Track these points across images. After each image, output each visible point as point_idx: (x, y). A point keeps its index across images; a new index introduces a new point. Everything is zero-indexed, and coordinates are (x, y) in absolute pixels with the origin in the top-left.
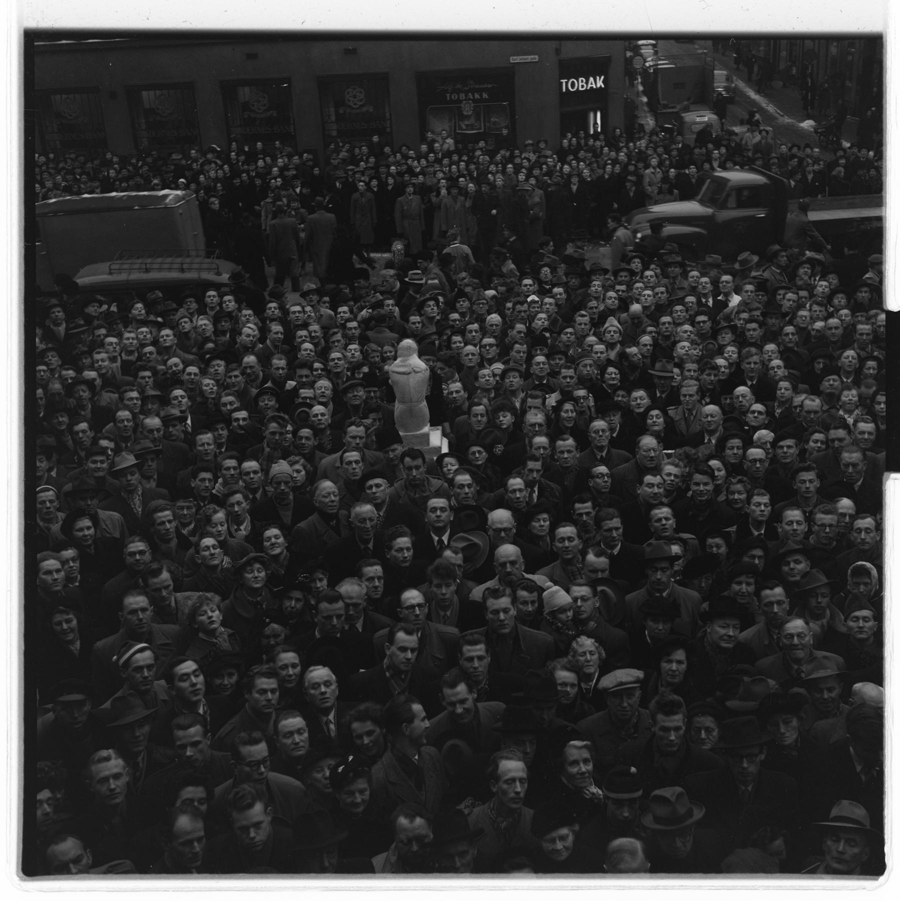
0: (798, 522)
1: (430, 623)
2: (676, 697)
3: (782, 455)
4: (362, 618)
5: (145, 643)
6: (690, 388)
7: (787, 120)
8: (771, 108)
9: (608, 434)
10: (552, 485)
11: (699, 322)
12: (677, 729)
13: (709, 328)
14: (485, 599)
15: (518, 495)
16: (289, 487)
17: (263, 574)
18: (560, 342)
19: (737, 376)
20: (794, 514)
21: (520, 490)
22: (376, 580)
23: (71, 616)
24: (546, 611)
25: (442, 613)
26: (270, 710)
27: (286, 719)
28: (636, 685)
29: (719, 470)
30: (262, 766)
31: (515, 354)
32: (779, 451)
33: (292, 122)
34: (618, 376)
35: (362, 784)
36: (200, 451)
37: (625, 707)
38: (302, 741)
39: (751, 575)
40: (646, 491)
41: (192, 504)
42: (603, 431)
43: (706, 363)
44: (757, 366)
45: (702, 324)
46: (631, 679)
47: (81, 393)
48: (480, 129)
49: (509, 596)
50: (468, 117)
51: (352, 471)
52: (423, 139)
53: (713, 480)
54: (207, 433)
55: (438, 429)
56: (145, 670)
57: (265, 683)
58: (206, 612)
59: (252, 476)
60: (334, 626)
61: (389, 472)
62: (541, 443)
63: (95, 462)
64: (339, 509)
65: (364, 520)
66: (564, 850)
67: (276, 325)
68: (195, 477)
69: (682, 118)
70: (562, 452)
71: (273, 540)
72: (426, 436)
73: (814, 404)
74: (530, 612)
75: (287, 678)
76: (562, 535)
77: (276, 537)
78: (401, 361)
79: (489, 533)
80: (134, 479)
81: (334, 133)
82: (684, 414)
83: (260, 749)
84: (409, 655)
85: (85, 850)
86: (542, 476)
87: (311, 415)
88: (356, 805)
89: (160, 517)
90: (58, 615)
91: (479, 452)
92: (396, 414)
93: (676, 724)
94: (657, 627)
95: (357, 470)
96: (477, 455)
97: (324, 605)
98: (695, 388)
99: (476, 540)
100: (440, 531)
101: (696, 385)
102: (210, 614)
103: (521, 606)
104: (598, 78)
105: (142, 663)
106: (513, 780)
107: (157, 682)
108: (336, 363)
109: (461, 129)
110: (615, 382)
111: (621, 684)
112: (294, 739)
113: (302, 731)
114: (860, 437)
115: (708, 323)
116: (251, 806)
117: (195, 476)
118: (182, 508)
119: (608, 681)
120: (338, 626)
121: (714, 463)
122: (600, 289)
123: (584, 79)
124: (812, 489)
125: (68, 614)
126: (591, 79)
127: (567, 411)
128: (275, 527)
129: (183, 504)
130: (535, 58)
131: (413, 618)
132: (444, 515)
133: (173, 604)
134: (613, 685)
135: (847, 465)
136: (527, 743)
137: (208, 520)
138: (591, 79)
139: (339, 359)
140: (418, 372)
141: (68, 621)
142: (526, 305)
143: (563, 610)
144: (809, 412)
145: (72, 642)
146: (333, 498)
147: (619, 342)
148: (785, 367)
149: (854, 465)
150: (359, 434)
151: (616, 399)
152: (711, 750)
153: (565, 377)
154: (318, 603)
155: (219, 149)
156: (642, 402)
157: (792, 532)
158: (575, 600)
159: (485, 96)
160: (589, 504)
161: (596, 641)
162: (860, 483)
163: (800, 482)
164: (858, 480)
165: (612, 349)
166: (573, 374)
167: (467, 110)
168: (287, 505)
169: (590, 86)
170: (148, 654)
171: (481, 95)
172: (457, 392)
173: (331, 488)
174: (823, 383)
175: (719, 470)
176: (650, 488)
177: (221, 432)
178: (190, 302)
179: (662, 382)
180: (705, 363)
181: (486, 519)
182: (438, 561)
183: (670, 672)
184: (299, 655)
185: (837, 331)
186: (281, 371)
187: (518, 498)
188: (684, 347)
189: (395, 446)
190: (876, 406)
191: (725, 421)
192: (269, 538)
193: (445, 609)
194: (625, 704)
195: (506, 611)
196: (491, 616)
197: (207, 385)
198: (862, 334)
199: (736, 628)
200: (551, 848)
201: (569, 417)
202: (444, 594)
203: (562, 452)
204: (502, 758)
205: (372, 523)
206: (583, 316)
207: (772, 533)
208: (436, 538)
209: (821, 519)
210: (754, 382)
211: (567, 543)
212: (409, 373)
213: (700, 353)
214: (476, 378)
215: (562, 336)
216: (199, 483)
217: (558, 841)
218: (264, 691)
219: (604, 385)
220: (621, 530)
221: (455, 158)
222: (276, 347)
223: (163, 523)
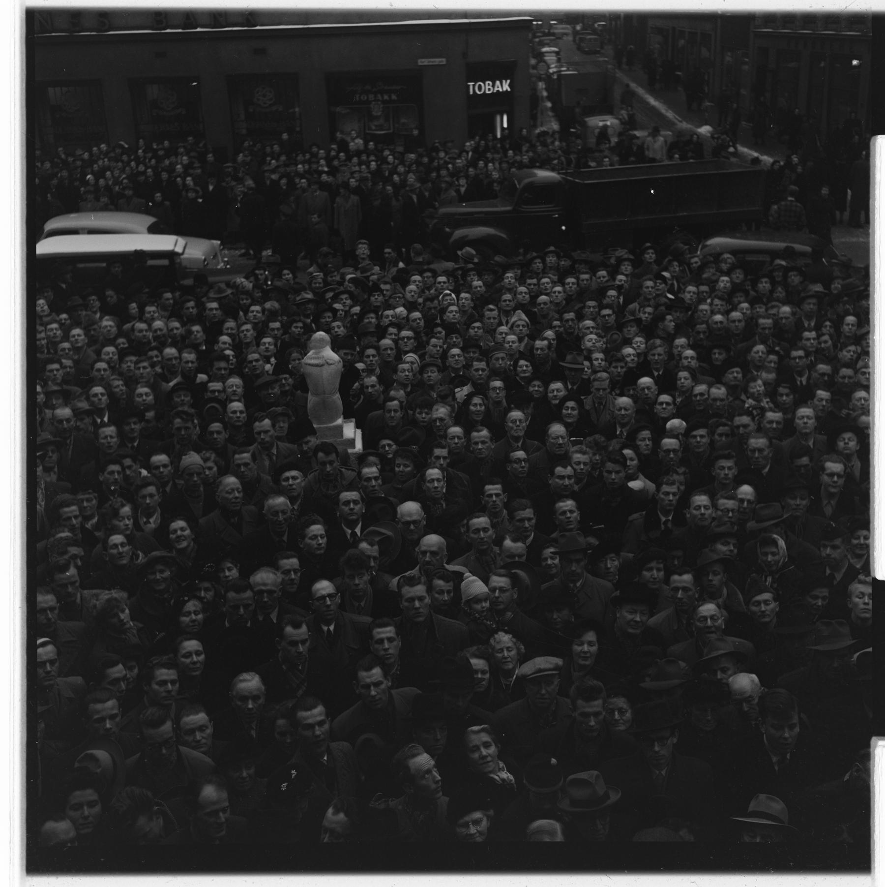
0: (705, 507)
2: (595, 682)
3: (696, 444)
4: (277, 610)
7: (685, 125)
8: (670, 114)
10: (461, 474)
12: (596, 714)
15: (436, 485)
19: (644, 367)
20: (701, 500)
22: (292, 573)
26: (170, 702)
28: (554, 672)
29: (632, 459)
31: (432, 348)
32: (693, 441)
36: (103, 444)
39: (661, 561)
40: (557, 482)
42: (520, 421)
44: (661, 357)
45: (607, 318)
46: (551, 666)
48: (389, 129)
49: (425, 584)
50: (377, 118)
52: (333, 139)
53: (625, 469)
55: (351, 422)
56: (48, 665)
57: (164, 674)
59: (162, 470)
61: (303, 464)
65: (276, 513)
66: (477, 835)
69: (585, 122)
70: (477, 443)
71: (179, 533)
72: (340, 429)
73: (720, 391)
74: (445, 601)
77: (182, 529)
78: (314, 353)
81: (244, 131)
82: (595, 405)
89: (67, 512)
91: (389, 445)
92: (309, 405)
93: (595, 709)
96: (387, 448)
97: (231, 595)
100: (352, 525)
103: (437, 596)
104: (504, 81)
109: (370, 129)
110: (527, 375)
111: (540, 670)
114: (768, 426)
117: (103, 470)
119: (528, 668)
121: (627, 452)
122: (513, 281)
123: (490, 83)
124: (730, 476)
126: (498, 83)
127: (476, 405)
128: (181, 519)
130: (442, 61)
132: (357, 508)
133: (78, 600)
135: (754, 450)
137: (116, 514)
138: (498, 83)
140: (331, 364)
143: (477, 599)
144: (715, 400)
146: (237, 495)
147: (527, 335)
148: (698, 359)
149: (760, 450)
151: (531, 389)
153: (477, 370)
155: (126, 146)
156: (559, 394)
157: (699, 516)
158: (493, 590)
159: (394, 97)
161: (514, 637)
162: (767, 470)
163: (719, 469)
164: (765, 467)
166: (485, 367)
167: (377, 111)
169: (496, 89)
171: (390, 97)
172: (373, 386)
173: (234, 483)
174: (726, 375)
175: (632, 459)
176: (561, 479)
177: (133, 426)
179: (573, 374)
180: (612, 353)
181: (395, 512)
182: (351, 551)
183: (583, 655)
185: (740, 324)
186: (190, 365)
188: (592, 339)
189: (309, 438)
190: (779, 398)
192: (175, 531)
194: (544, 692)
195: (421, 599)
196: (406, 604)
198: (764, 329)
201: (478, 411)
202: (357, 585)
203: (477, 443)
205: (285, 516)
206: (491, 310)
207: (680, 519)
208: (350, 531)
209: (724, 504)
210: (661, 373)
211: (482, 534)
212: (322, 365)
213: (604, 346)
214: (395, 371)
215: (471, 330)
216: (108, 476)
217: (471, 826)
218: (164, 683)
219: (518, 378)
220: (534, 521)
221: (364, 157)
223: (69, 518)
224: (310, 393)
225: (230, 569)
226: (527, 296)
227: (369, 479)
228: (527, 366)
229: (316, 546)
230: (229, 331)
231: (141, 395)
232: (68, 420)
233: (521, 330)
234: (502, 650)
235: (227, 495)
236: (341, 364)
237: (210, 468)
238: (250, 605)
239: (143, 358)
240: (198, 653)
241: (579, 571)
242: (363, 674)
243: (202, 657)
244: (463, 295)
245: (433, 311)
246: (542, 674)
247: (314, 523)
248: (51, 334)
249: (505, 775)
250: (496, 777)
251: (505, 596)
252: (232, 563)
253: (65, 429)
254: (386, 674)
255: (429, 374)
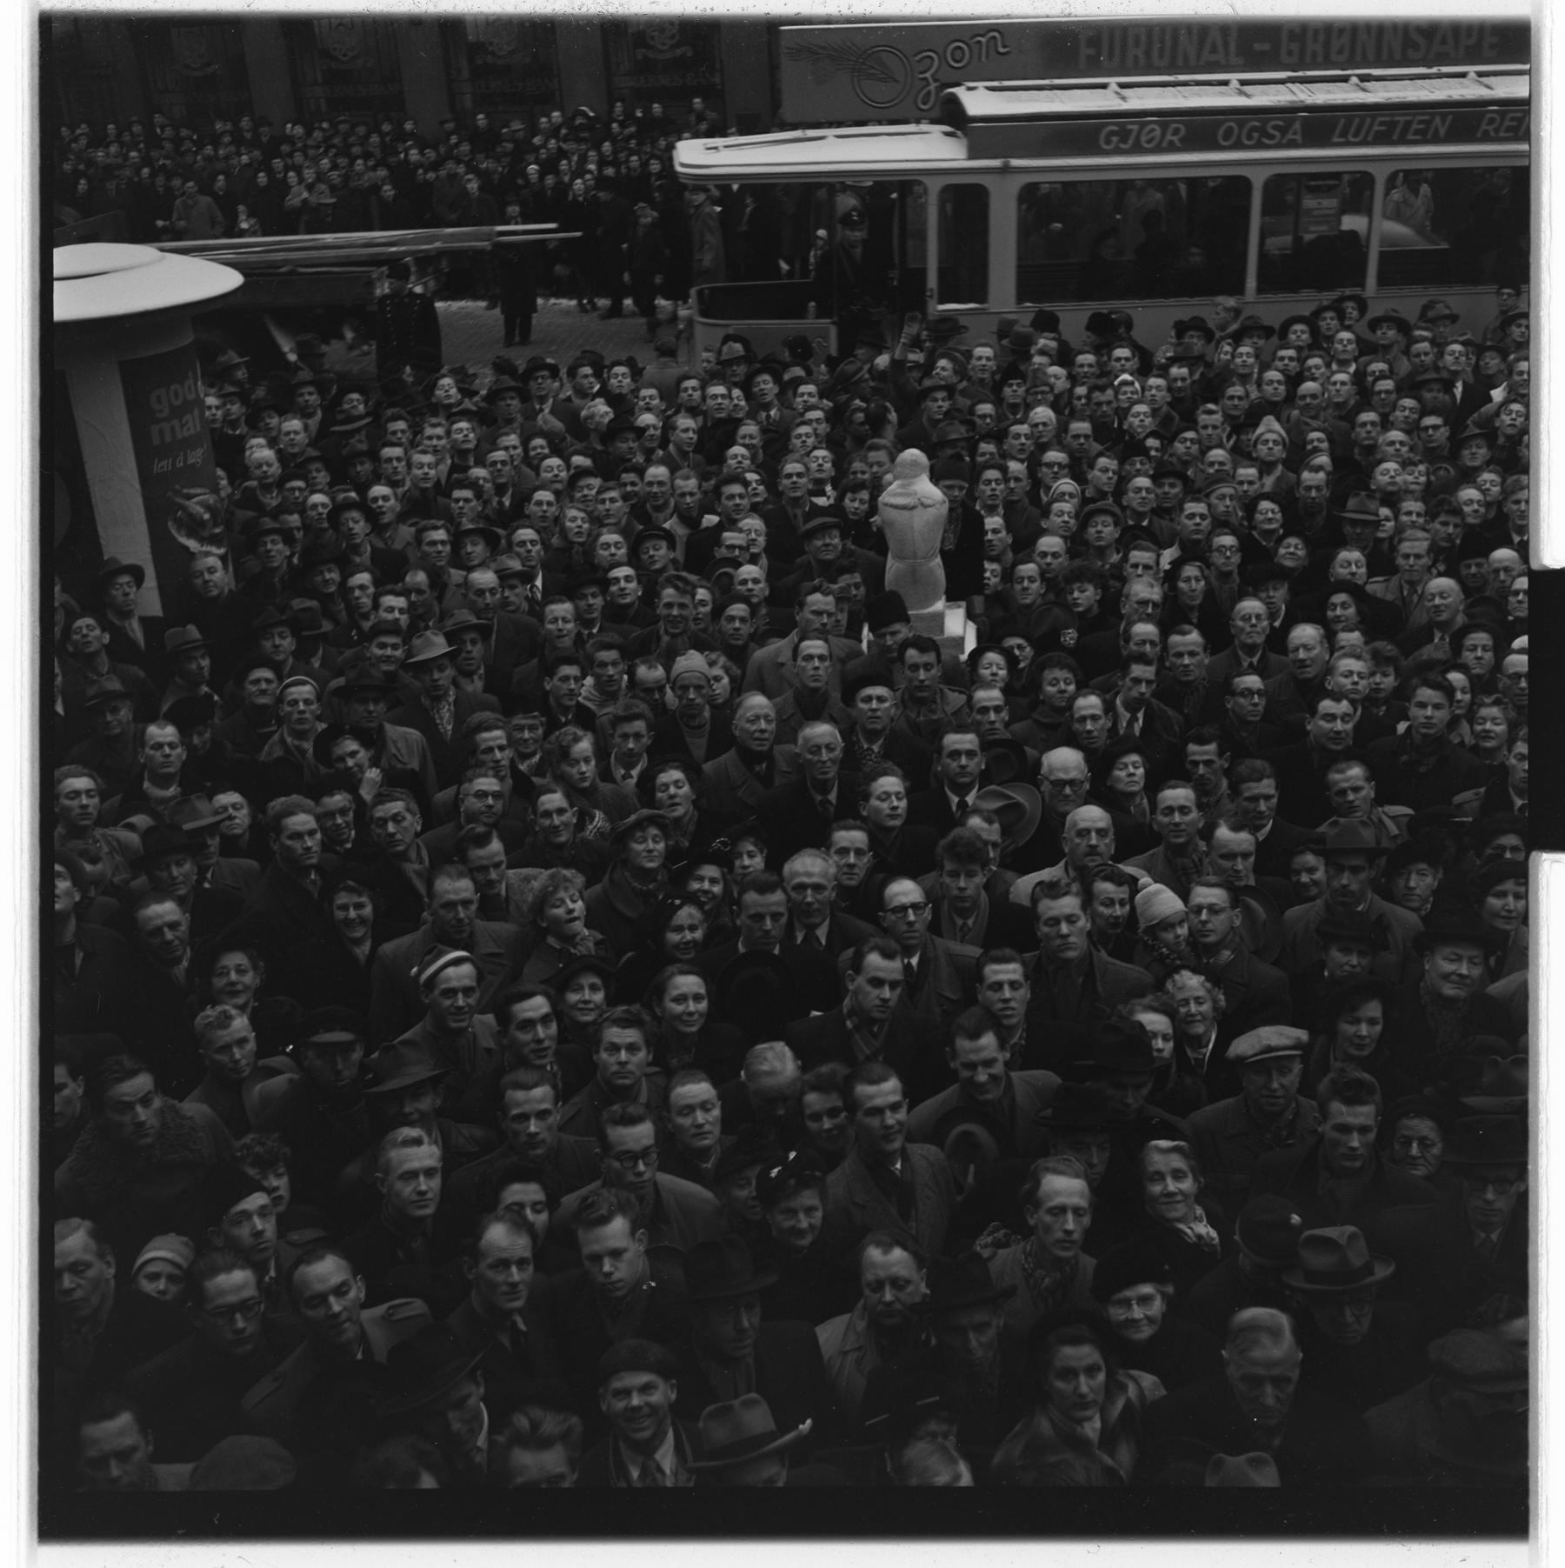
1: (938, 940)
2: (1366, 1076)
5: (463, 949)
6: (1415, 545)
9: (1265, 623)
11: (1427, 428)
12: (1363, 1130)
13: (1444, 438)
14: (1034, 900)
16: (703, 696)
17: (661, 846)
18: (1171, 455)
21: (1094, 718)
23: (364, 899)
24: (1142, 926)
25: (960, 922)
27: (683, 1084)
30: (640, 1162)
31: (1098, 473)
33: (718, 66)
34: (1279, 516)
35: (809, 1198)
36: (550, 631)
37: (1275, 1091)
38: (708, 1122)
40: (1321, 727)
41: (537, 722)
42: (1258, 617)
43: (1441, 503)
45: (1430, 432)
46: (1285, 1042)
47: (351, 524)
49: (1077, 894)
51: (812, 672)
54: (563, 602)
55: (959, 607)
58: (563, 901)
60: (767, 932)
62: (1146, 633)
63: (383, 646)
64: (774, 743)
66: (1145, 1322)
67: (684, 417)
68: (551, 674)
70: (1180, 655)
72: (939, 618)
75: (685, 1018)
76: (1169, 803)
77: (676, 783)
79: (1042, 789)
80: (444, 676)
82: (1402, 593)
83: (642, 1134)
84: (886, 993)
85: (355, 1276)
86: (1154, 695)
87: (736, 581)
88: (801, 1233)
89: (486, 740)
90: (343, 894)
92: (889, 576)
93: (1361, 1120)
94: (1341, 961)
95: (820, 672)
97: (751, 897)
98: (1426, 544)
99: (1020, 799)
100: (962, 790)
101: (1426, 539)
102: (571, 906)
105: (455, 984)
106: (1062, 1209)
107: (480, 1017)
108: (795, 483)
111: (1269, 1049)
112: (695, 1119)
113: (709, 1106)
115: (1442, 430)
116: (605, 1220)
118: (521, 728)
119: (1245, 1045)
120: (774, 933)
125: (360, 895)
127: (1188, 579)
128: (676, 768)
129: (524, 722)
131: (905, 928)
133: (503, 893)
134: (1255, 1051)
136: (1094, 1149)
139: (799, 475)
140: (929, 506)
141: (359, 906)
142: (1110, 392)
143: (1167, 924)
145: (358, 942)
150: (828, 608)
152: (1427, 1178)
154: (741, 893)
155: (592, 114)
160: (1212, 747)
161: (1207, 980)
165: (1269, 473)
168: (700, 726)
170: (466, 969)
173: (761, 707)
176: (1328, 721)
177: (591, 601)
178: (543, 377)
179: (1358, 531)
180: (1438, 499)
182: (957, 832)
183: (1357, 1041)
184: (705, 980)
186: (688, 499)
187: (1089, 732)
188: (1388, 471)
189: (897, 627)
191: (1469, 607)
193: (964, 913)
194: (1275, 1085)
195: (1071, 919)
196: (1046, 929)
197: (574, 519)
199: (1476, 964)
200: (1123, 1317)
204: (1048, 1170)
206: (1211, 412)
208: (955, 799)
212: (913, 508)
216: (559, 683)
217: (1135, 1307)
220: (1275, 800)
222: (684, 454)
223: (491, 750)
224: (890, 556)
225: (751, 855)
226: (1282, 388)
227: (985, 710)
228: (1273, 511)
229: (888, 811)
230: (747, 441)
231: (607, 546)
232: (492, 591)
233: (1270, 449)
234: (1186, 1002)
235: (748, 725)
236: (946, 506)
237: (717, 679)
238: (781, 914)
239: (611, 484)
240: (697, 998)
241: (1354, 887)
242: (963, 1043)
243: (703, 1006)
244: (1153, 381)
245: (1105, 408)
246: (1273, 1054)
247: (885, 774)
248: (460, 437)
249: (1203, 1229)
250: (1188, 1231)
251: (1219, 923)
252: (756, 845)
253: (487, 605)
254: (1002, 1043)
255: (1100, 528)
